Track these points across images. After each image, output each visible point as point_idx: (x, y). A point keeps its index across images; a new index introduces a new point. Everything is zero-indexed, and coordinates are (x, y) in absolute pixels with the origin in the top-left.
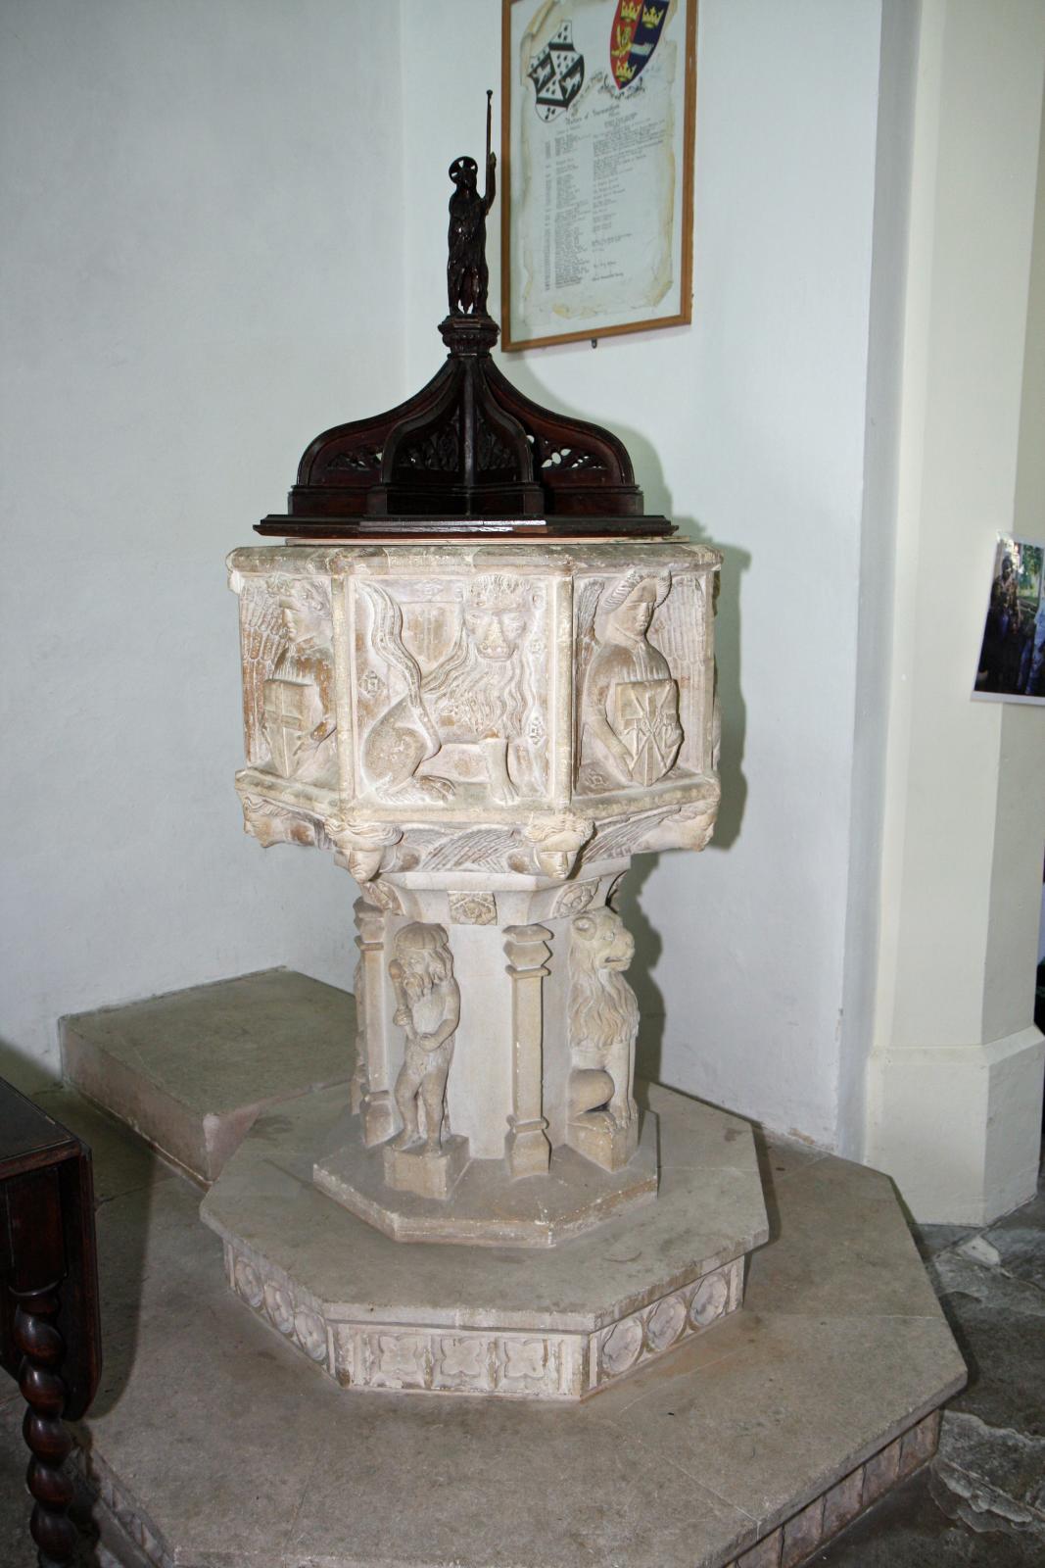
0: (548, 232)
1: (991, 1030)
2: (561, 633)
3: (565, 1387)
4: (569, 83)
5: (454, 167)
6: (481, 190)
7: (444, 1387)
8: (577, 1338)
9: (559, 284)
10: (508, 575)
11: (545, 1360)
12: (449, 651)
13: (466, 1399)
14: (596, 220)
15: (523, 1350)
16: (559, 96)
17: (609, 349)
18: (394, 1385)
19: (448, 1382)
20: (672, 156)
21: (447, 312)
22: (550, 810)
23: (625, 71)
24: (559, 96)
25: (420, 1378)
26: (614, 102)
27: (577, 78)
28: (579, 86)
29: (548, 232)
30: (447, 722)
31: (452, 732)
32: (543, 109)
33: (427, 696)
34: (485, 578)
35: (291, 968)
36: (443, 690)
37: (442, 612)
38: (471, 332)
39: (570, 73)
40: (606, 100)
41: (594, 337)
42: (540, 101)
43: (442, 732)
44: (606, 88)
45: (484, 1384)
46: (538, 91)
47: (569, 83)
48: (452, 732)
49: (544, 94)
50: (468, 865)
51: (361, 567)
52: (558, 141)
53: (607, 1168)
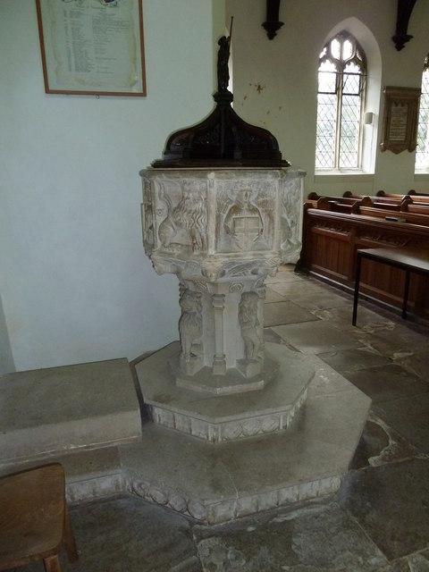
38: (222, 97)
41: (98, 94)
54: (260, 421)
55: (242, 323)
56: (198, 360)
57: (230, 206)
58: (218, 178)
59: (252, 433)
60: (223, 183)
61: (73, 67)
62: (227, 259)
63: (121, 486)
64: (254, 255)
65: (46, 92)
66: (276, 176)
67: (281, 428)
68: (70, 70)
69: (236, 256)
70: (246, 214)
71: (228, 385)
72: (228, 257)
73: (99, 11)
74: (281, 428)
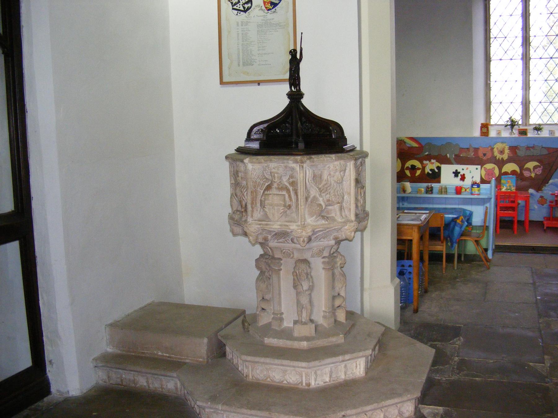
0: (239, 49)
1: (392, 279)
2: (353, 177)
3: (361, 373)
4: (246, 6)
5: (290, 52)
6: (298, 57)
7: (333, 381)
8: (364, 359)
9: (244, 65)
10: (342, 162)
11: (356, 367)
12: (324, 183)
13: (340, 382)
14: (259, 47)
15: (352, 365)
16: (242, 8)
17: (263, 88)
18: (321, 384)
19: (334, 379)
20: (289, 34)
21: (289, 90)
22: (352, 221)
23: (269, 6)
24: (242, 8)
25: (327, 380)
26: (266, 14)
27: (249, 5)
28: (250, 7)
29: (239, 49)
30: (328, 201)
31: (329, 203)
32: (236, 12)
33: (322, 194)
34: (337, 163)
35: (156, 301)
36: (326, 192)
37: (322, 172)
38: (295, 97)
39: (247, 3)
40: (261, 13)
41: (259, 83)
42: (233, 9)
43: (327, 203)
44: (261, 9)
45: (343, 377)
46: (233, 6)
47: (246, 6)
48: (329, 203)
49: (235, 7)
50: (322, 240)
51: (308, 161)
52: (242, 22)
53: (344, 321)
54: (285, 372)
55: (295, 287)
56: (266, 313)
57: (267, 184)
58: (251, 163)
59: (278, 381)
60: (257, 166)
61: (241, 63)
62: (259, 226)
63: (179, 390)
64: (280, 225)
65: (221, 84)
66: (296, 162)
67: (304, 384)
68: (239, 65)
69: (267, 225)
70: (274, 191)
71: (274, 338)
72: (260, 224)
73: (262, 18)
74: (304, 384)
